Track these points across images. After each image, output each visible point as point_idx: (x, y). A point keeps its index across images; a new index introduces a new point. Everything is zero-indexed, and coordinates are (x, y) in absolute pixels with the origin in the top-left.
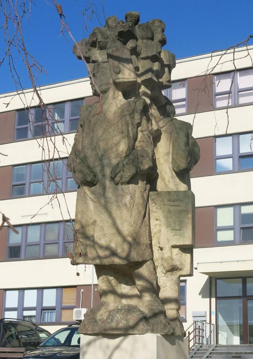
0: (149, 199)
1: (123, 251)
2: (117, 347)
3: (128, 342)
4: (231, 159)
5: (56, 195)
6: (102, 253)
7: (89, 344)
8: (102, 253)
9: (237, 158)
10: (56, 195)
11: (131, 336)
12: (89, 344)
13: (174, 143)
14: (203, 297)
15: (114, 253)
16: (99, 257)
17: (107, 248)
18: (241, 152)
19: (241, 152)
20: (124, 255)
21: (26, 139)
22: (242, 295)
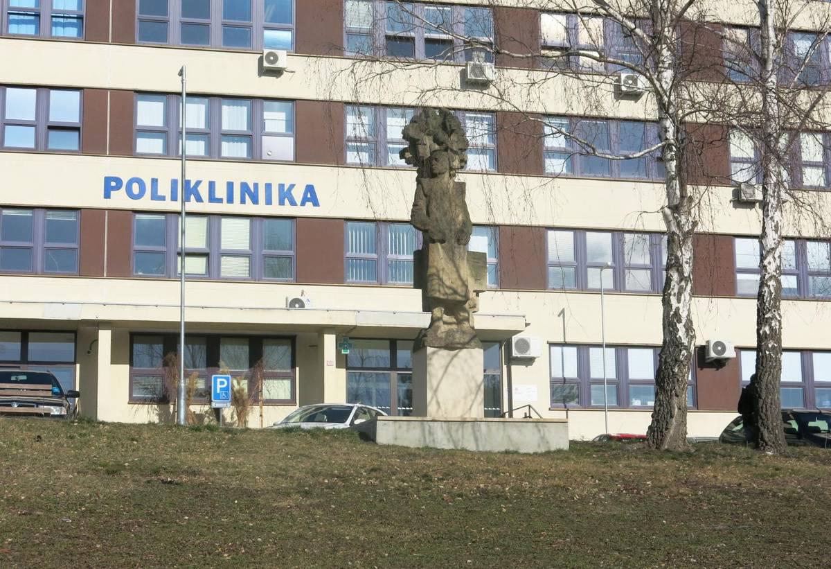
0: (664, 285)
1: (462, 291)
2: (456, 355)
3: (464, 353)
4: (33, 128)
5: (644, 268)
6: (449, 291)
7: (434, 353)
8: (449, 291)
9: (43, 128)
10: (644, 268)
11: (465, 350)
12: (434, 353)
13: (676, 215)
14: (743, 389)
15: (455, 292)
16: (446, 294)
17: (450, 288)
18: (7, 118)
19: (7, 118)
20: (463, 294)
21: (164, 44)
22: (420, 291)
